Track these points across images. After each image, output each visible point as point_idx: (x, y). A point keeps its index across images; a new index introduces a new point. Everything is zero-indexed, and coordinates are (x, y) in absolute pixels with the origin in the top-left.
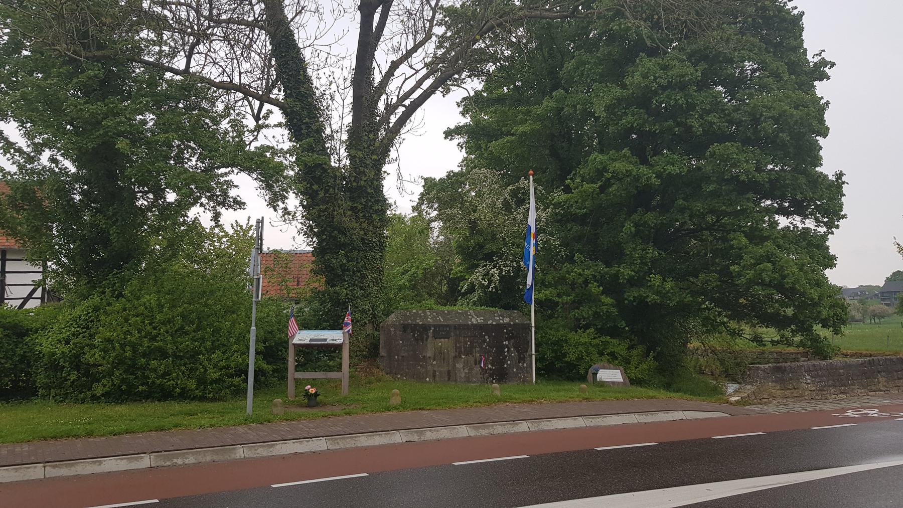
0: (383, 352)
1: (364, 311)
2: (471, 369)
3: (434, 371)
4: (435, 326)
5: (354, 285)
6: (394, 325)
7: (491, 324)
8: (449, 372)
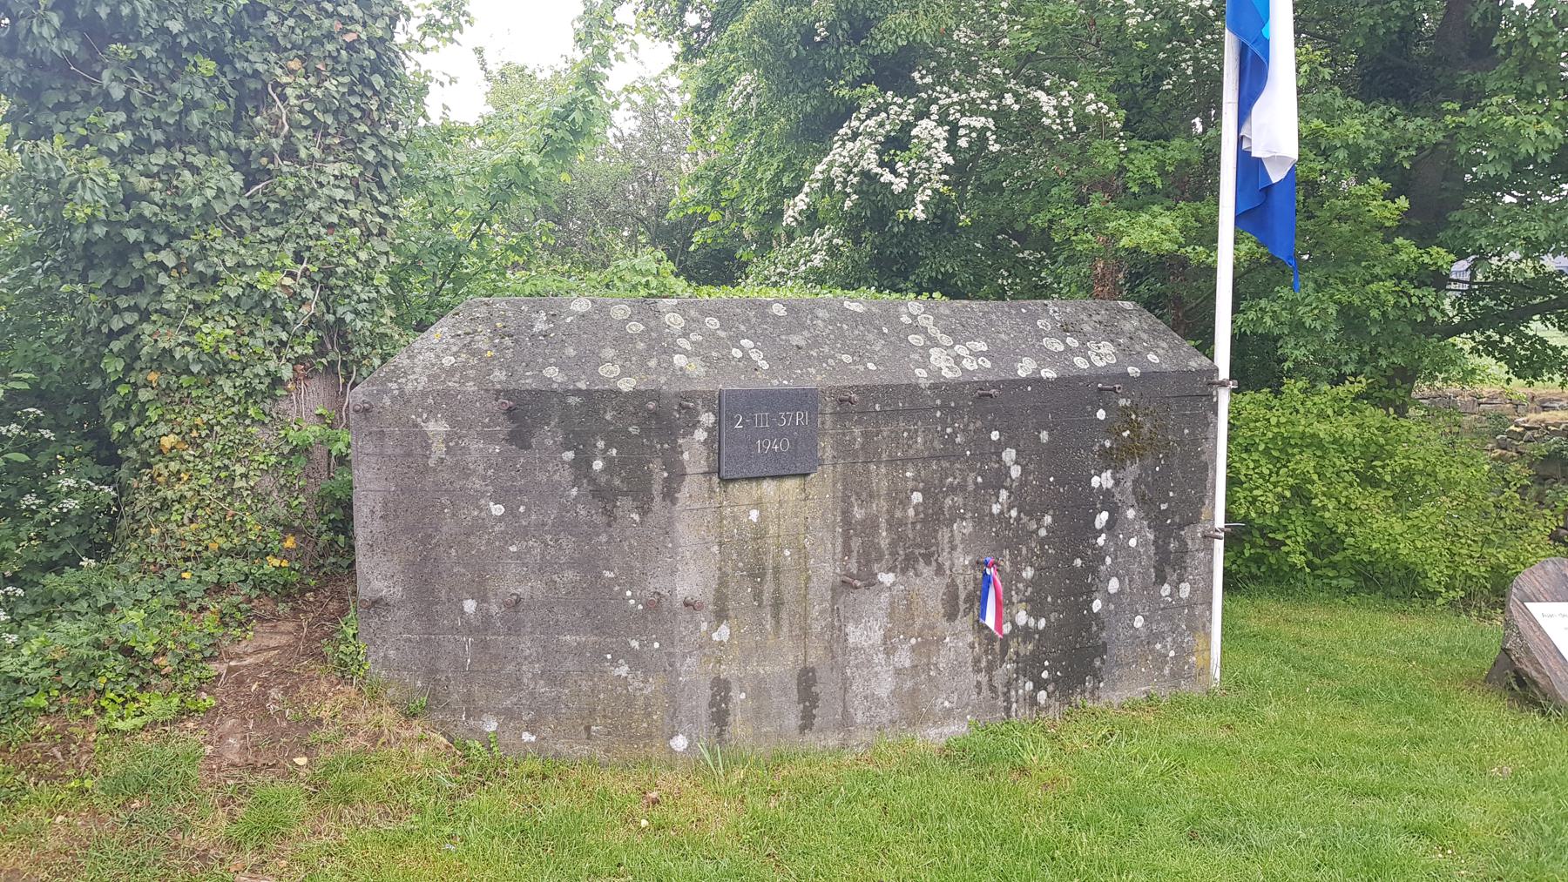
0: (377, 575)
1: (261, 307)
2: (928, 645)
3: (721, 687)
4: (724, 405)
5: (179, 137)
6: (443, 401)
7: (1037, 381)
8: (807, 679)
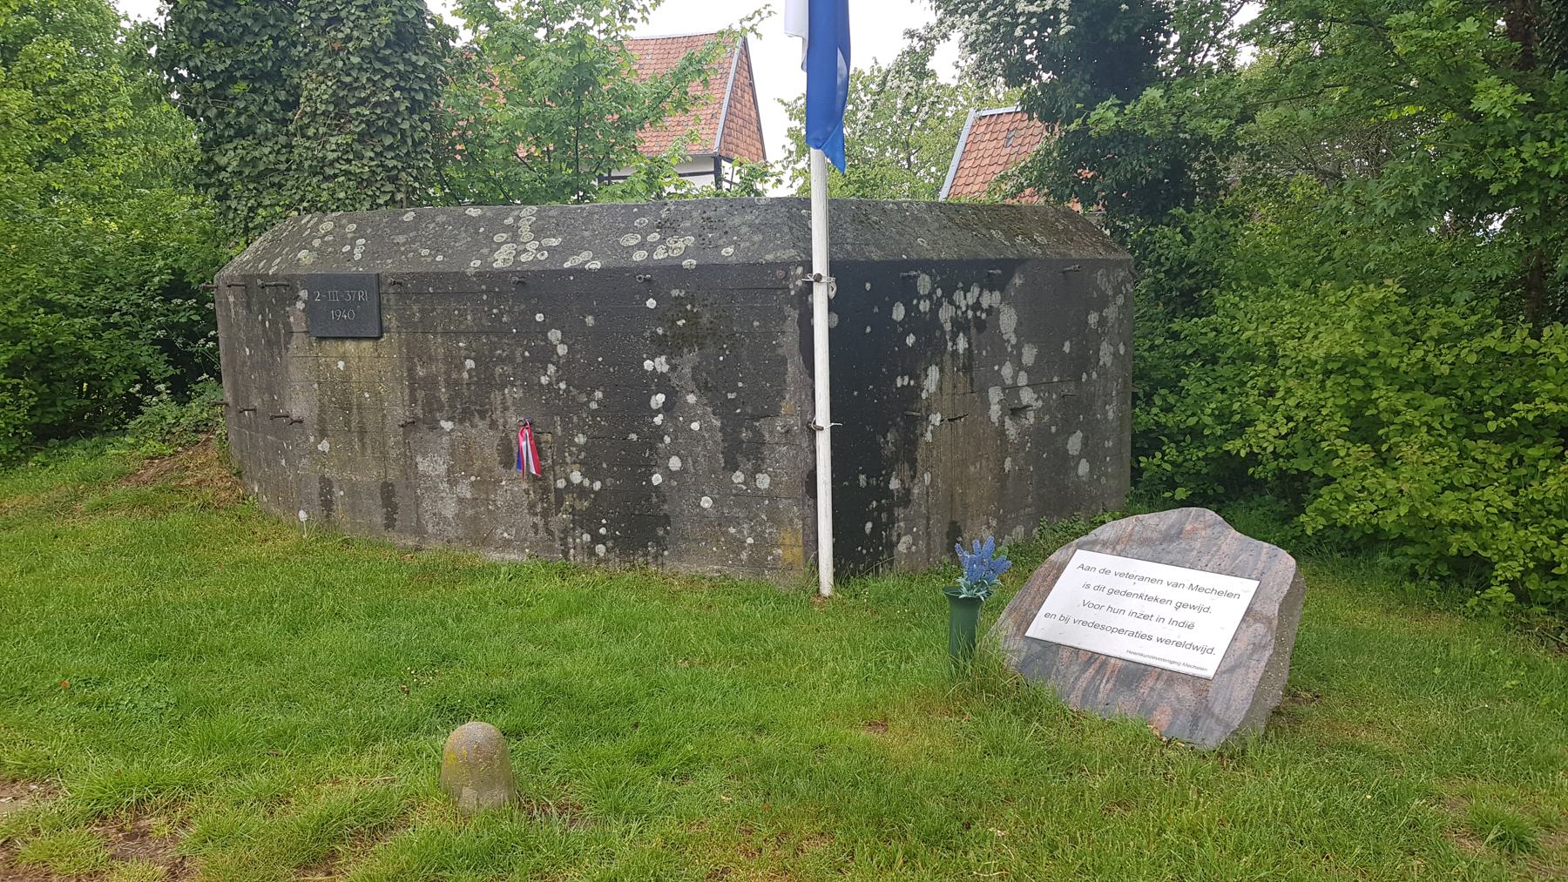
2: (486, 484)
4: (311, 282)
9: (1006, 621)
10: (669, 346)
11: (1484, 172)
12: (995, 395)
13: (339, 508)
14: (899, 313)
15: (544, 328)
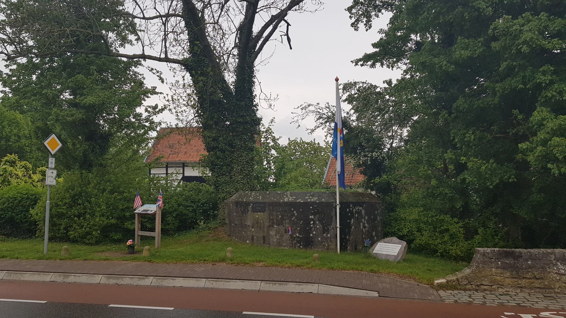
2: (282, 236)
3: (253, 236)
4: (253, 203)
9: (371, 250)
10: (314, 214)
11: (435, 192)
12: (361, 224)
13: (255, 240)
14: (348, 210)
15: (293, 211)
